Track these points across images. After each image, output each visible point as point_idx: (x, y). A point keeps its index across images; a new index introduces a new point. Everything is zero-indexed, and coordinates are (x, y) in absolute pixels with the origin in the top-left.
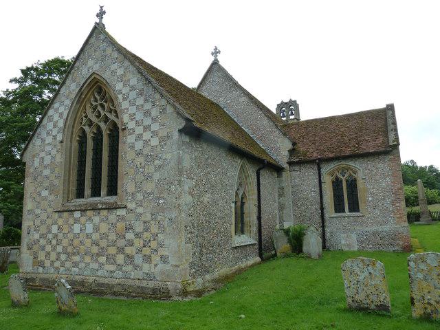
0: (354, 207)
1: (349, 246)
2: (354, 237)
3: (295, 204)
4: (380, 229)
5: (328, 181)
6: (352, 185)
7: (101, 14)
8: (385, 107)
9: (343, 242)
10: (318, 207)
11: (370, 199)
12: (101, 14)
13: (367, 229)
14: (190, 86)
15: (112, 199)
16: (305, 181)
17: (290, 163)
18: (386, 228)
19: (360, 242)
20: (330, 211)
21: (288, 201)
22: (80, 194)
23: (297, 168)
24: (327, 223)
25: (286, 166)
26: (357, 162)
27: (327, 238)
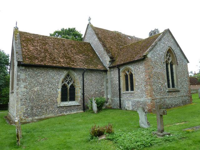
0: (132, 89)
1: (129, 107)
2: (130, 103)
3: (112, 87)
4: (139, 100)
5: (122, 75)
6: (131, 75)
7: (90, 19)
8: (144, 35)
9: (127, 106)
10: (118, 88)
11: (137, 84)
12: (90, 19)
13: (135, 100)
14: (148, 37)
15: (132, 92)
16: (114, 75)
17: (110, 68)
18: (142, 100)
19: (132, 106)
20: (123, 91)
21: (109, 85)
22: (127, 90)
23: (112, 70)
24: (122, 96)
25: (108, 69)
26: (132, 66)
27: (122, 103)
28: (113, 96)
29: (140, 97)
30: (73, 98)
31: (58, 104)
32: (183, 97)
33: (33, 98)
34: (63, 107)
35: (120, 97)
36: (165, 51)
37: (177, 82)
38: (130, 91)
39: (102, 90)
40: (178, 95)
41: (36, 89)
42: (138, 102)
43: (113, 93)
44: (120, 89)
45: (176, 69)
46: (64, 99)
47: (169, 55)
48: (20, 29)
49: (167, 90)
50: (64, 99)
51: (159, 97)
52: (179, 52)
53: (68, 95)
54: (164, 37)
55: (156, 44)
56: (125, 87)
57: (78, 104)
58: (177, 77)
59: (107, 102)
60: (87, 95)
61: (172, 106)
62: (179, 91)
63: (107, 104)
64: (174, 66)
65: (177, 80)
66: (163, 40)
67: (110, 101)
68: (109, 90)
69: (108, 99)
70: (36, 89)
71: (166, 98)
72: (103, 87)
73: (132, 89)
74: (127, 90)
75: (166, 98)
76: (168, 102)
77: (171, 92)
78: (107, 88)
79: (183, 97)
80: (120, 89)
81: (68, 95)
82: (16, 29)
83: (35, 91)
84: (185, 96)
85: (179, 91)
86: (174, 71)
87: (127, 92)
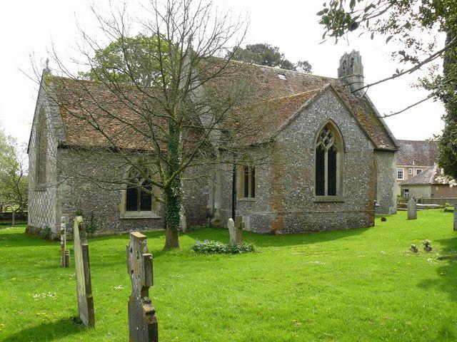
13: (255, 213)
19: (251, 224)
22: (246, 195)
28: (223, 206)
29: (264, 209)
30: (147, 206)
31: (122, 213)
32: (352, 214)
33: (80, 202)
34: (130, 219)
35: (234, 209)
36: (317, 128)
37: (341, 186)
38: (326, 197)
39: (204, 193)
40: (337, 209)
41: (85, 187)
42: (259, 217)
43: (224, 199)
44: (234, 193)
45: (342, 161)
46: (131, 206)
47: (327, 134)
48: (56, 72)
49: (315, 200)
50: (131, 206)
51: (294, 210)
52: (352, 128)
53: (139, 199)
54: (319, 101)
55: (298, 116)
56: (244, 188)
57: (156, 216)
58: (341, 176)
59: (212, 217)
60: (386, 315)
61: (321, 228)
62: (343, 202)
63: (213, 220)
64: (338, 155)
65: (341, 181)
66: (314, 108)
67: (219, 214)
68: (218, 193)
69: (215, 210)
70: (85, 187)
71: (310, 213)
72: (207, 187)
73: (253, 196)
74: (246, 195)
75: (310, 213)
76: (312, 219)
77: (324, 202)
78: (214, 190)
79: (352, 214)
80: (234, 193)
81: (139, 199)
82: (47, 72)
83: (84, 192)
84: (356, 212)
85: (343, 202)
86: (338, 164)
87: (246, 199)
